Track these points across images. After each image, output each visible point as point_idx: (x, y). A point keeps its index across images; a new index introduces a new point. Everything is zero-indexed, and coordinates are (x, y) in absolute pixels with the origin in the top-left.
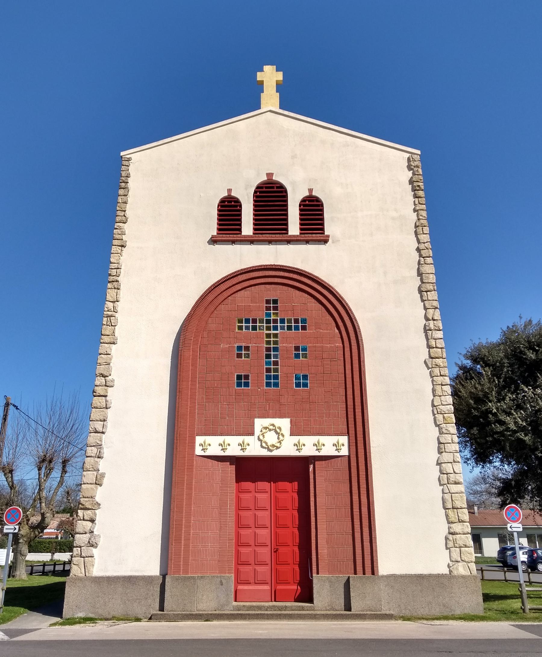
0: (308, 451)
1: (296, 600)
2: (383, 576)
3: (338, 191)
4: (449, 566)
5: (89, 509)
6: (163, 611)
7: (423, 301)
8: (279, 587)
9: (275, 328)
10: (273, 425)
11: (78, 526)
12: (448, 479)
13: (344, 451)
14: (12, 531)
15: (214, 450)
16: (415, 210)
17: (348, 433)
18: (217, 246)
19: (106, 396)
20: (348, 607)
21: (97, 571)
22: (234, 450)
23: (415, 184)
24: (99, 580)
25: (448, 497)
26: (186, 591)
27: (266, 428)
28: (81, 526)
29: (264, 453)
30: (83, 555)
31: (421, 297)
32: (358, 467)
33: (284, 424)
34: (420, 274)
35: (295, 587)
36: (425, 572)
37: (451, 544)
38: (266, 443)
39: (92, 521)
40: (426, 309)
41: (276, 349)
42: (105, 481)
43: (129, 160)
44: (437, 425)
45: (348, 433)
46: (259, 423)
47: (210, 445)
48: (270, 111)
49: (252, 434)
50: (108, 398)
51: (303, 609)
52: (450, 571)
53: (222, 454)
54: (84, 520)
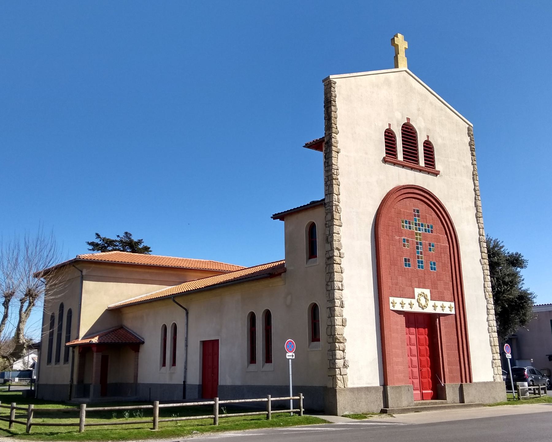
0: (439, 311)
1: (432, 399)
2: (475, 383)
3: (440, 141)
4: (494, 377)
5: (341, 343)
6: (464, 403)
7: (478, 223)
8: (423, 392)
9: (419, 230)
10: (423, 293)
11: (337, 354)
12: (492, 329)
13: (453, 312)
14: (291, 357)
15: (398, 308)
16: (473, 164)
17: (454, 300)
18: (387, 166)
19: (340, 264)
20: (462, 400)
21: (350, 385)
22: (407, 308)
23: (472, 146)
24: (352, 390)
25: (492, 339)
26: (398, 395)
27: (420, 295)
28: (339, 354)
29: (420, 310)
30: (342, 373)
31: (477, 220)
32: (460, 320)
33: (427, 292)
34: (476, 206)
35: (430, 391)
36: (486, 381)
37: (494, 366)
38: (421, 304)
39: (343, 351)
40: (479, 228)
41: (421, 244)
42: (348, 323)
43: (335, 83)
44: (486, 299)
45: (454, 300)
46: (418, 291)
47: (397, 303)
48: (406, 71)
49: (414, 298)
50: (341, 265)
51: (436, 403)
52: (494, 380)
53: (401, 309)
54: (339, 350)
